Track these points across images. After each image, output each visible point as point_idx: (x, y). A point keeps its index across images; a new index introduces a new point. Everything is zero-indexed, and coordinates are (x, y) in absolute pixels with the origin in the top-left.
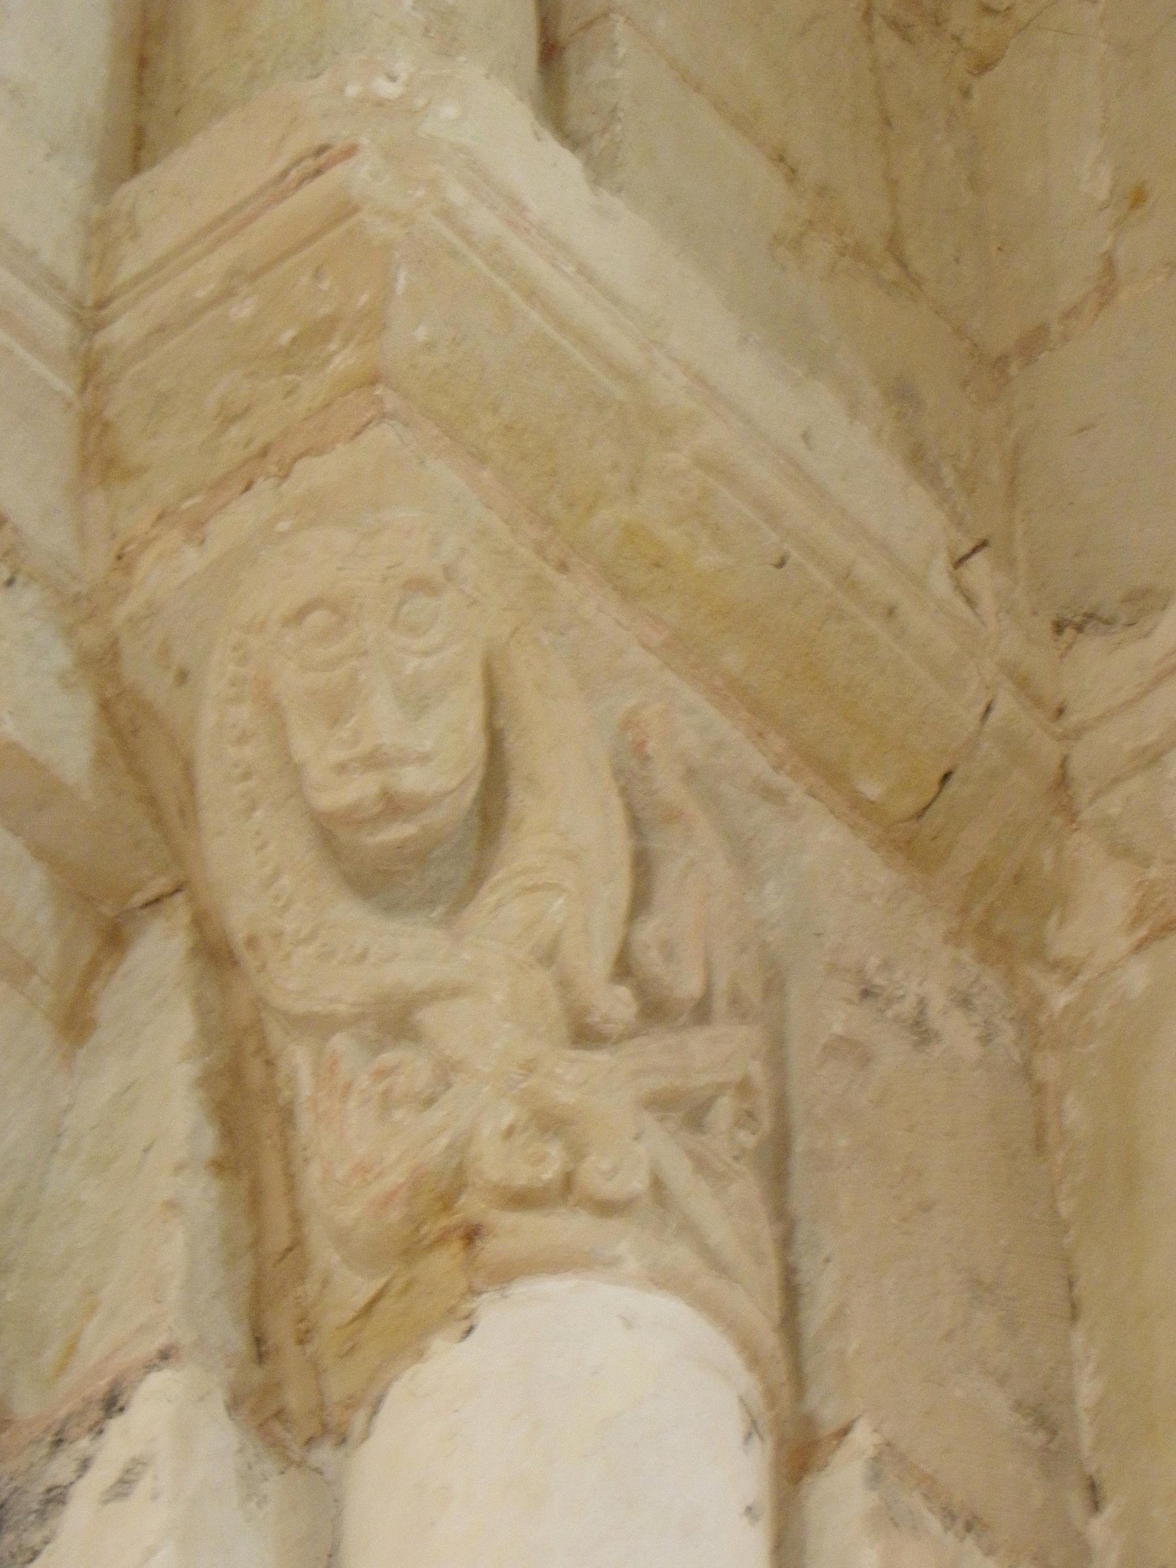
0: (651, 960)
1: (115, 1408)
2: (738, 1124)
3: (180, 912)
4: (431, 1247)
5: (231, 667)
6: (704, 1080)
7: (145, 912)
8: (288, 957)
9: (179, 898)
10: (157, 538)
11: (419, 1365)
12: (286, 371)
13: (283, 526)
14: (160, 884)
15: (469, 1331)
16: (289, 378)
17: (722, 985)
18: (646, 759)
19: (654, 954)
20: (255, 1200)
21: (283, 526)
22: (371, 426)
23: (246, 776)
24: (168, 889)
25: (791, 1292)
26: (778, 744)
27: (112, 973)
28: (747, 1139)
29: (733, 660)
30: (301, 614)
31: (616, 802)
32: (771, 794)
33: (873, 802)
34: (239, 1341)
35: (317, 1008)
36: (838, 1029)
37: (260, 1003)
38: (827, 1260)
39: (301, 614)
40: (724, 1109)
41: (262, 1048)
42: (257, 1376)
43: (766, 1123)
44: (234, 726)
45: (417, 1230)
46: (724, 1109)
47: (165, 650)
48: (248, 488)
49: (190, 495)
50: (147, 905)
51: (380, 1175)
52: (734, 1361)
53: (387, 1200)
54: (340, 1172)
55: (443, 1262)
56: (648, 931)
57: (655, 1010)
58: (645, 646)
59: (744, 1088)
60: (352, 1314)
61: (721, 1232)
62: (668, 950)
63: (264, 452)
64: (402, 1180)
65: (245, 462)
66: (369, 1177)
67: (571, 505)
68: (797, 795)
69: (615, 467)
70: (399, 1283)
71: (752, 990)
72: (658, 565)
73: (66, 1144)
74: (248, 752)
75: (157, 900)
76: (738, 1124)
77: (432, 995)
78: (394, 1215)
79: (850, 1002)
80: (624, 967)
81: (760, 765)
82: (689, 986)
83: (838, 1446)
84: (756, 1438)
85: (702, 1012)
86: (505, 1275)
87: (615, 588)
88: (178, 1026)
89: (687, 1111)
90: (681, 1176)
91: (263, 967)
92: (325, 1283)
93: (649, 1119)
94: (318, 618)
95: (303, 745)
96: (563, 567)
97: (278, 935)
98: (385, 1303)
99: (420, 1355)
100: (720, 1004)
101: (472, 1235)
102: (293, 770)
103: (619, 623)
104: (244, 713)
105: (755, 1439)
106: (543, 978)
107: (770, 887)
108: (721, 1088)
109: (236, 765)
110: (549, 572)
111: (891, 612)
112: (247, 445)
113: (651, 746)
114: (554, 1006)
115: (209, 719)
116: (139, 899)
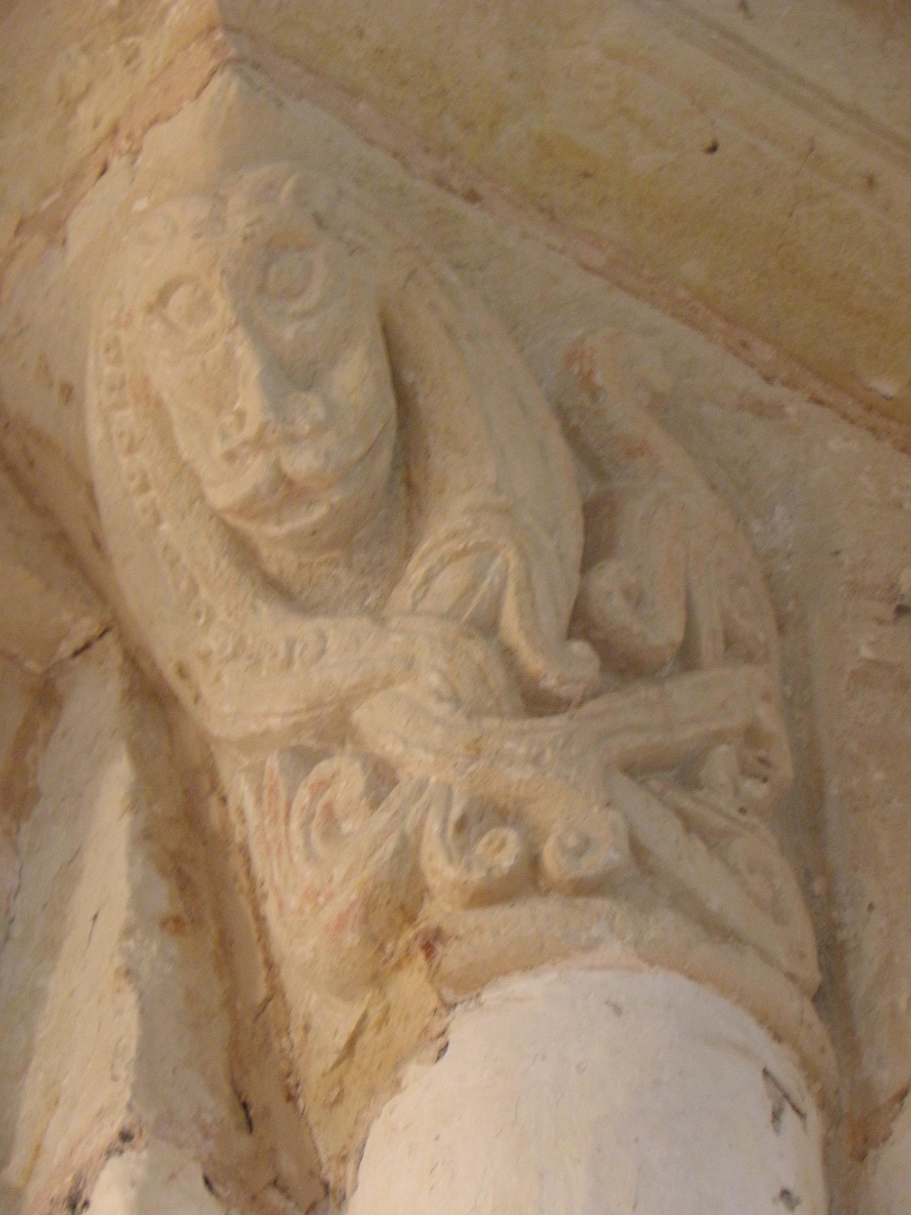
0: (614, 610)
1: (79, 1205)
2: (746, 771)
3: (111, 653)
4: (398, 966)
5: (108, 370)
6: (691, 732)
7: (78, 659)
8: (218, 678)
9: (109, 638)
10: (21, 246)
11: (397, 1098)
12: (122, 36)
13: (141, 205)
14: (86, 627)
15: (444, 1049)
16: (129, 41)
17: (709, 622)
18: (595, 393)
19: (618, 601)
20: (226, 954)
21: (141, 205)
22: (216, 75)
23: (145, 487)
24: (96, 631)
25: (832, 951)
26: (766, 353)
27: (48, 735)
28: (757, 790)
29: (693, 269)
30: (163, 296)
31: (556, 442)
32: (763, 410)
33: (891, 399)
34: (218, 1109)
35: (253, 727)
36: (866, 652)
37: (205, 740)
38: (871, 907)
39: (163, 296)
40: (721, 763)
41: (215, 785)
42: (243, 1143)
43: (785, 768)
44: (121, 435)
45: (382, 948)
46: (721, 763)
47: (45, 369)
48: (104, 171)
49: (47, 193)
50: (76, 653)
51: (330, 897)
52: (758, 1037)
53: (341, 924)
54: (293, 903)
55: (411, 984)
56: (608, 579)
57: (623, 665)
58: (587, 268)
59: (752, 735)
60: (335, 1057)
61: (721, 896)
62: (636, 598)
63: (115, 130)
64: (354, 897)
65: (98, 145)
66: (321, 899)
67: (469, 126)
68: (795, 407)
69: (513, 76)
70: (375, 1015)
71: (758, 629)
72: (586, 175)
73: (17, 930)
74: (141, 458)
75: (87, 646)
76: (746, 771)
77: (364, 690)
78: (351, 938)
79: (881, 622)
80: (581, 622)
81: (745, 380)
82: (667, 631)
83: (900, 1110)
84: (789, 1117)
85: (687, 657)
86: (471, 983)
87: (541, 210)
88: (118, 778)
89: (671, 771)
90: (665, 838)
91: (197, 698)
92: (306, 1028)
93: (622, 782)
94: (180, 298)
95: (186, 443)
96: (472, 197)
97: (205, 657)
98: (367, 1038)
99: (397, 1086)
100: (709, 646)
101: (430, 944)
102: (185, 473)
103: (550, 247)
104: (127, 417)
105: (789, 1117)
106: (477, 650)
107: (780, 511)
108: (719, 737)
109: (132, 478)
110: (456, 204)
111: (871, 182)
112: (96, 125)
113: (598, 379)
114: (498, 678)
115: (96, 434)
116: (66, 649)
